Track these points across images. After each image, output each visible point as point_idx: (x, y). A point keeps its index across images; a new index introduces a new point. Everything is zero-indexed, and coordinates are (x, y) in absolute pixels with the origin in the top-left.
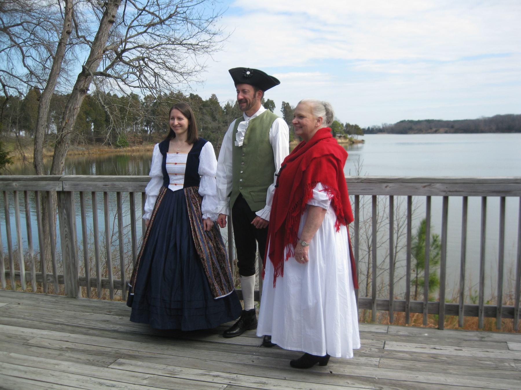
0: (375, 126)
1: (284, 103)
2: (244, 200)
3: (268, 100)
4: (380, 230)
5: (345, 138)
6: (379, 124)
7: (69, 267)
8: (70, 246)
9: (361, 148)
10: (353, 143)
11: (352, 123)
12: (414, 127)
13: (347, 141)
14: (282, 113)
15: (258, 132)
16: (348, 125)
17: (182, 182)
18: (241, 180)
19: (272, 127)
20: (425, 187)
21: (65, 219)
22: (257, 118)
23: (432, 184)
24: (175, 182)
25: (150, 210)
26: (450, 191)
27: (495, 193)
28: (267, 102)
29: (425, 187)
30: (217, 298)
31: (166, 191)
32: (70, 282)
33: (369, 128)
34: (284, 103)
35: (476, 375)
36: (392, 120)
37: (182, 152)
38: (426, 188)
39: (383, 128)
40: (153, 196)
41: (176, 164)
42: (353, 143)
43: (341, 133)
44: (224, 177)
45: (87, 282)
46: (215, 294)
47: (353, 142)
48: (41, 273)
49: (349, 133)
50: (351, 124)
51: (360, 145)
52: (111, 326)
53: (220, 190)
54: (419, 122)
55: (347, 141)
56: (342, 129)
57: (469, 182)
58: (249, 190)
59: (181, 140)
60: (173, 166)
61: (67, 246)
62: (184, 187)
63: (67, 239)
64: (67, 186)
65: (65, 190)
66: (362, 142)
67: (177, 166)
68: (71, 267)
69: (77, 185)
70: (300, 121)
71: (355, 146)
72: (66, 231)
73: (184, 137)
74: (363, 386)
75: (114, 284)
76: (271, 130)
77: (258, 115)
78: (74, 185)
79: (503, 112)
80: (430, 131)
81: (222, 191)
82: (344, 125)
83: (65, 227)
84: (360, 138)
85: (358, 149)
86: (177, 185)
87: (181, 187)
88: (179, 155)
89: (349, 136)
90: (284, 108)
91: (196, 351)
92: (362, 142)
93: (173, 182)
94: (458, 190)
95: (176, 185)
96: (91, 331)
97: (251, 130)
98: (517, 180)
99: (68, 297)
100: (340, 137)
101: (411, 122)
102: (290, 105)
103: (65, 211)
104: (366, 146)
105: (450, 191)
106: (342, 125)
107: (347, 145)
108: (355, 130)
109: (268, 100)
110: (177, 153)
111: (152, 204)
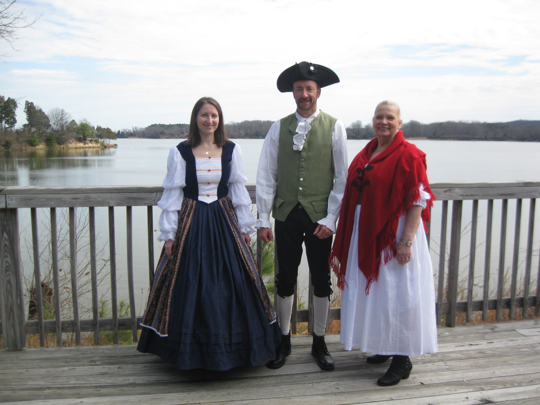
0: (125, 130)
1: (27, 103)
2: (303, 210)
3: (9, 98)
4: (98, 237)
5: (97, 142)
6: (129, 127)
7: (12, 310)
8: (13, 282)
9: (114, 153)
10: (105, 147)
11: (104, 126)
12: (165, 131)
13: (99, 145)
14: (25, 114)
15: (319, 134)
16: (99, 129)
17: (215, 192)
18: (301, 189)
19: (334, 130)
20: (445, 192)
21: (6, 245)
22: (315, 119)
23: (452, 189)
24: (207, 192)
25: (173, 229)
26: (467, 195)
27: (498, 196)
28: (7, 101)
29: (445, 192)
30: (272, 323)
31: (196, 204)
32: (12, 331)
33: (119, 131)
34: (27, 103)
35: (531, 362)
36: (143, 124)
37: (214, 156)
38: (447, 193)
39: (134, 131)
40: (173, 212)
41: (209, 170)
42: (105, 147)
43: (92, 136)
44: (268, 186)
45: (41, 327)
46: (270, 319)
47: (105, 147)
48: (55, 319)
49: (101, 137)
50: (103, 127)
51: (112, 150)
52: (120, 379)
53: (265, 200)
54: (170, 126)
55: (99, 145)
56: (93, 132)
57: (477, 186)
58: (310, 199)
59: (208, 142)
60: (206, 173)
61: (9, 282)
62: (219, 198)
63: (8, 273)
64: (13, 202)
65: (9, 207)
66: (115, 146)
67: (210, 173)
68: (15, 309)
69: (31, 199)
70: (391, 122)
71: (107, 151)
72: (7, 262)
73: (211, 138)
74: (467, 390)
75: (81, 325)
76: (333, 133)
77: (316, 116)
78: (26, 200)
79: (251, 119)
80: (182, 135)
81: (267, 202)
82: (96, 128)
83: (6, 256)
84: (112, 142)
85: (110, 154)
86: (208, 196)
87: (215, 198)
88: (211, 159)
89: (100, 140)
90: (28, 108)
91: (224, 392)
92: (115, 146)
93: (204, 193)
94: (473, 194)
95: (208, 196)
96: (103, 391)
97: (312, 133)
98: (519, 183)
99: (8, 351)
100: (91, 141)
101: (163, 126)
102: (35, 105)
103: (5, 235)
104: (119, 152)
105: (467, 195)
106: (93, 128)
107: (99, 149)
108: (106, 133)
109: (9, 98)
110: (210, 158)
111: (175, 221)
